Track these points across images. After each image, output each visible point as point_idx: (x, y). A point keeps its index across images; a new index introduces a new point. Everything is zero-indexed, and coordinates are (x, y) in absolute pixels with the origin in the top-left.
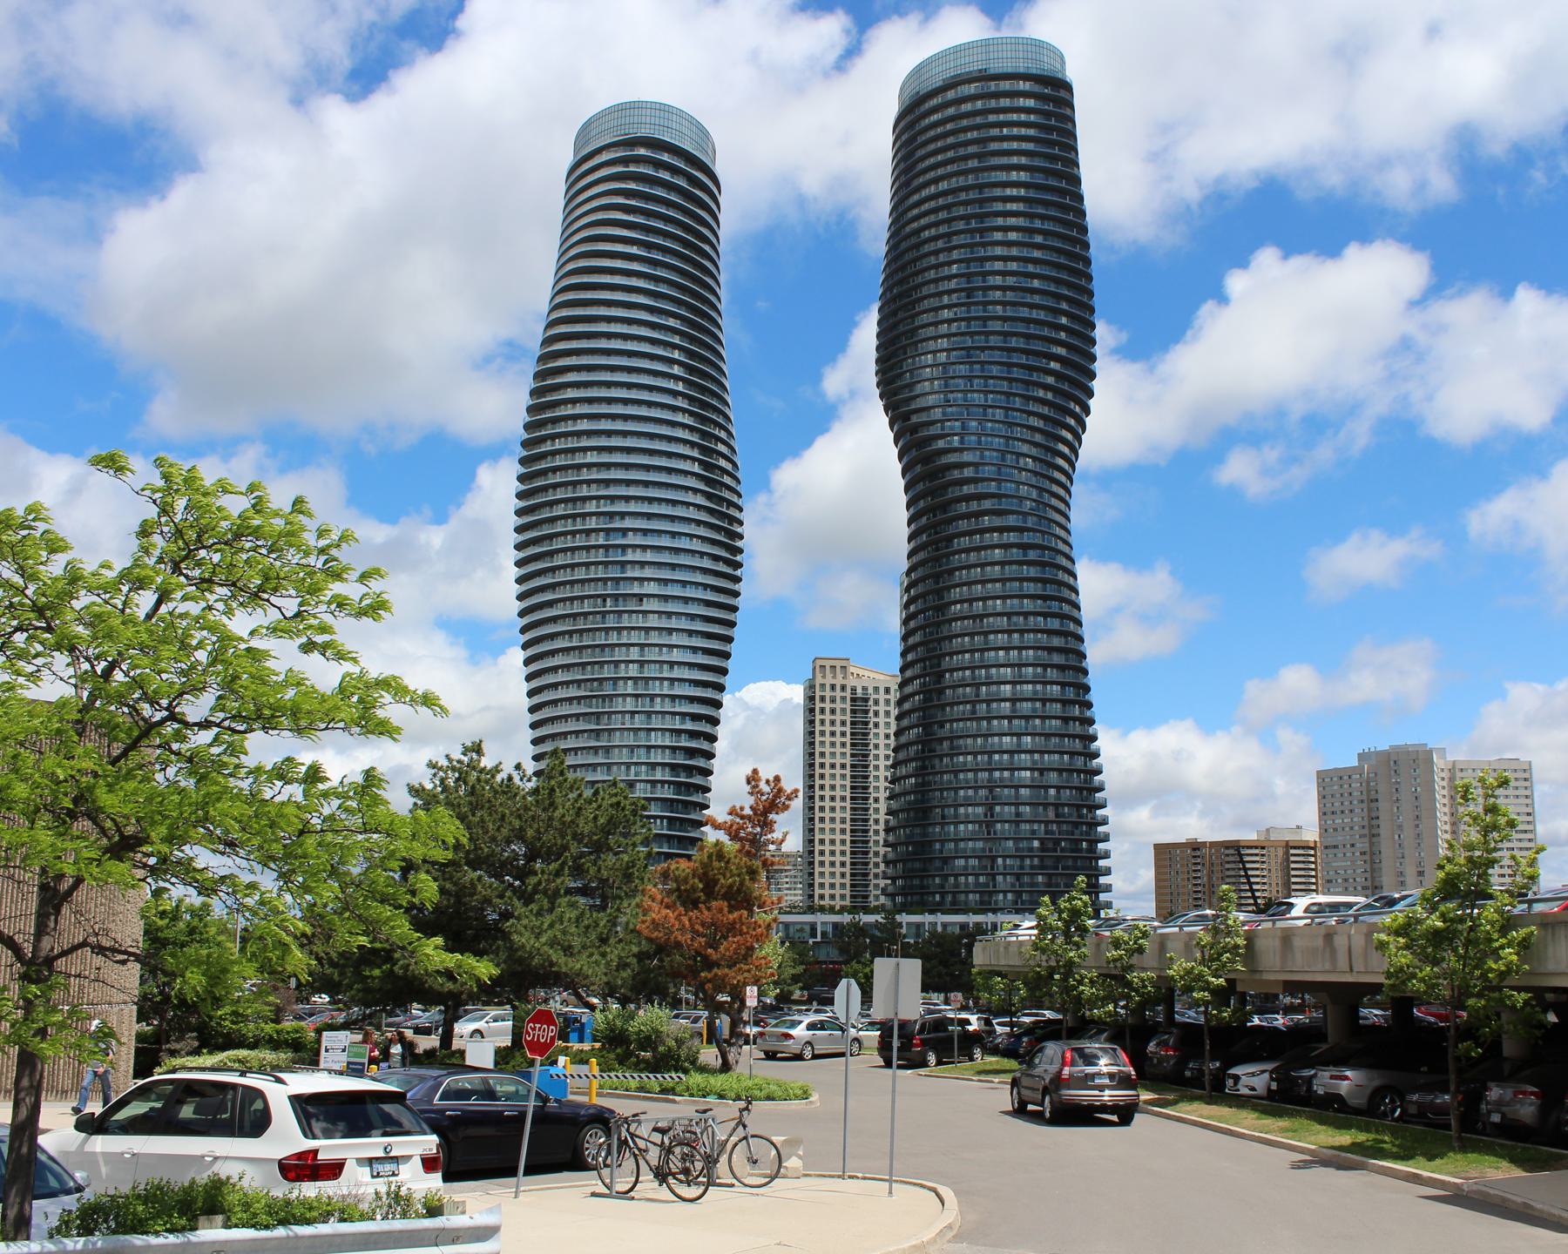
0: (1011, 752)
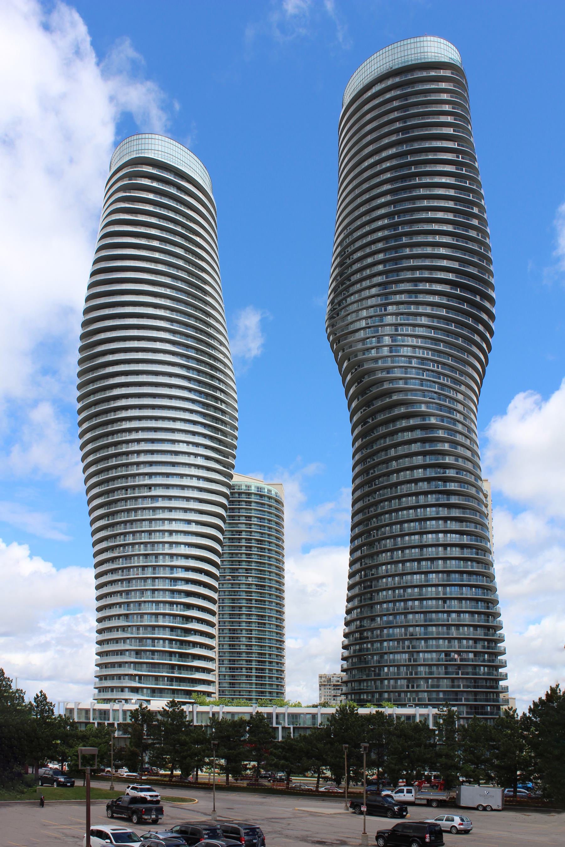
0: (420, 587)
